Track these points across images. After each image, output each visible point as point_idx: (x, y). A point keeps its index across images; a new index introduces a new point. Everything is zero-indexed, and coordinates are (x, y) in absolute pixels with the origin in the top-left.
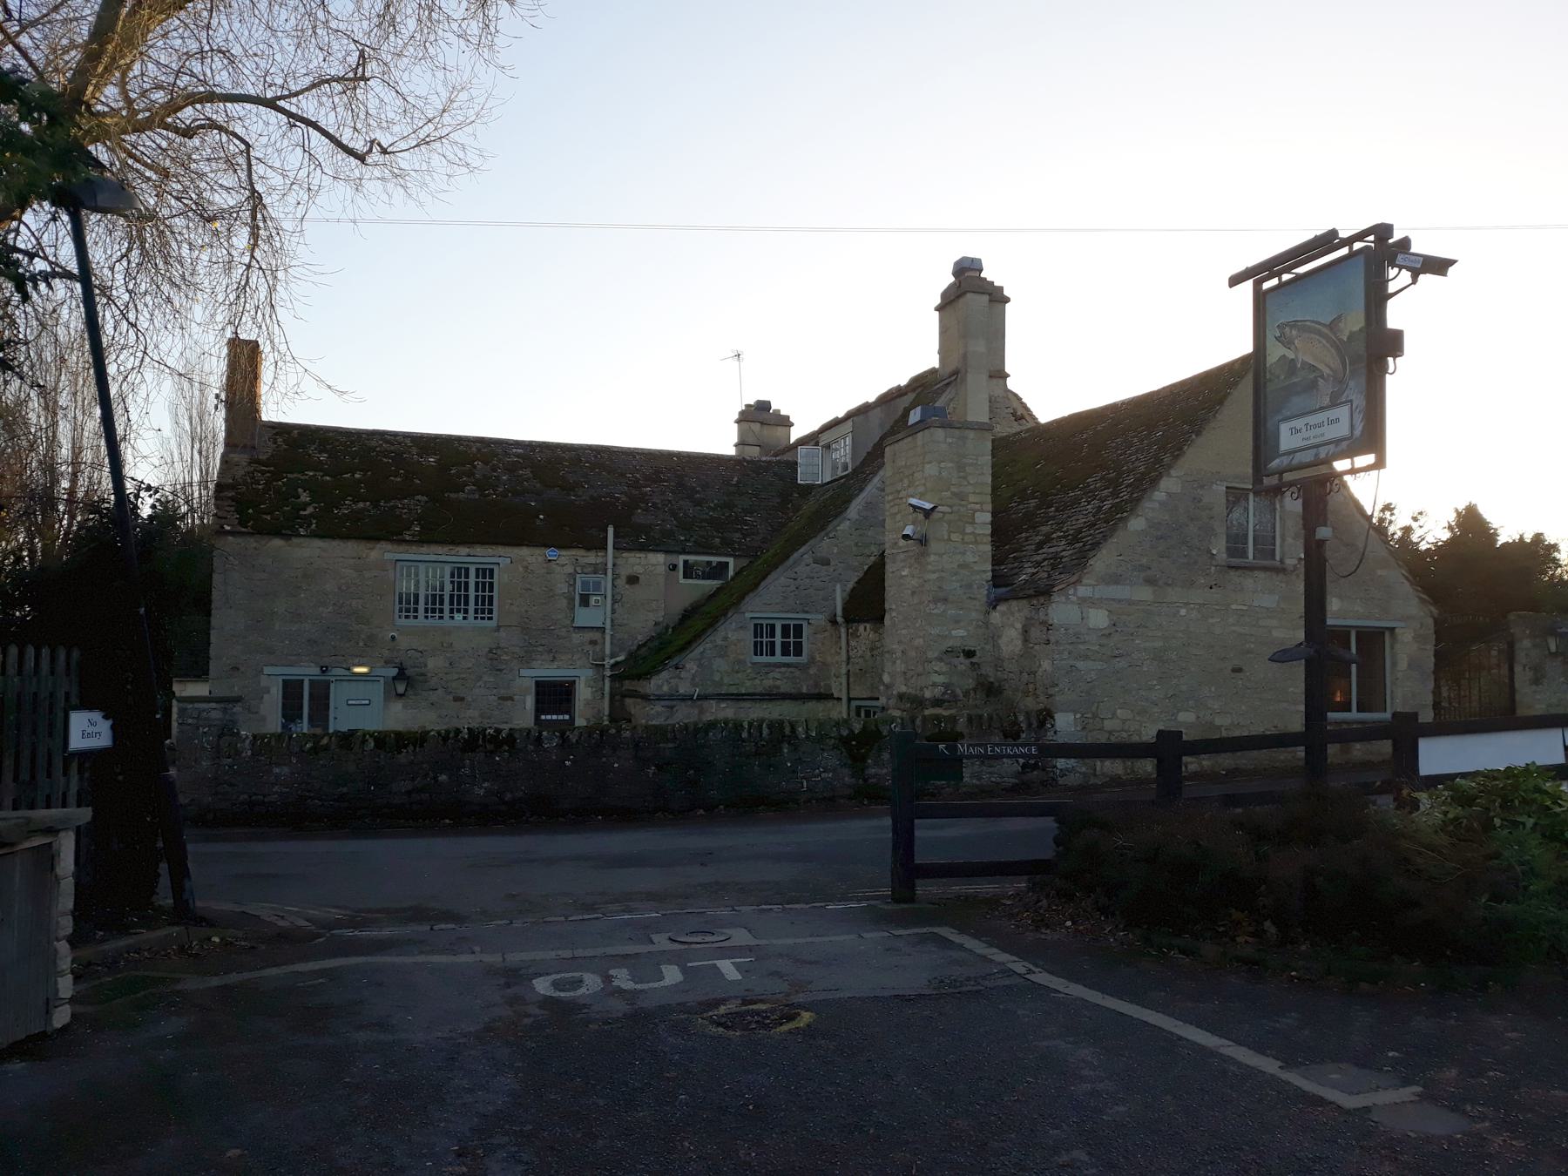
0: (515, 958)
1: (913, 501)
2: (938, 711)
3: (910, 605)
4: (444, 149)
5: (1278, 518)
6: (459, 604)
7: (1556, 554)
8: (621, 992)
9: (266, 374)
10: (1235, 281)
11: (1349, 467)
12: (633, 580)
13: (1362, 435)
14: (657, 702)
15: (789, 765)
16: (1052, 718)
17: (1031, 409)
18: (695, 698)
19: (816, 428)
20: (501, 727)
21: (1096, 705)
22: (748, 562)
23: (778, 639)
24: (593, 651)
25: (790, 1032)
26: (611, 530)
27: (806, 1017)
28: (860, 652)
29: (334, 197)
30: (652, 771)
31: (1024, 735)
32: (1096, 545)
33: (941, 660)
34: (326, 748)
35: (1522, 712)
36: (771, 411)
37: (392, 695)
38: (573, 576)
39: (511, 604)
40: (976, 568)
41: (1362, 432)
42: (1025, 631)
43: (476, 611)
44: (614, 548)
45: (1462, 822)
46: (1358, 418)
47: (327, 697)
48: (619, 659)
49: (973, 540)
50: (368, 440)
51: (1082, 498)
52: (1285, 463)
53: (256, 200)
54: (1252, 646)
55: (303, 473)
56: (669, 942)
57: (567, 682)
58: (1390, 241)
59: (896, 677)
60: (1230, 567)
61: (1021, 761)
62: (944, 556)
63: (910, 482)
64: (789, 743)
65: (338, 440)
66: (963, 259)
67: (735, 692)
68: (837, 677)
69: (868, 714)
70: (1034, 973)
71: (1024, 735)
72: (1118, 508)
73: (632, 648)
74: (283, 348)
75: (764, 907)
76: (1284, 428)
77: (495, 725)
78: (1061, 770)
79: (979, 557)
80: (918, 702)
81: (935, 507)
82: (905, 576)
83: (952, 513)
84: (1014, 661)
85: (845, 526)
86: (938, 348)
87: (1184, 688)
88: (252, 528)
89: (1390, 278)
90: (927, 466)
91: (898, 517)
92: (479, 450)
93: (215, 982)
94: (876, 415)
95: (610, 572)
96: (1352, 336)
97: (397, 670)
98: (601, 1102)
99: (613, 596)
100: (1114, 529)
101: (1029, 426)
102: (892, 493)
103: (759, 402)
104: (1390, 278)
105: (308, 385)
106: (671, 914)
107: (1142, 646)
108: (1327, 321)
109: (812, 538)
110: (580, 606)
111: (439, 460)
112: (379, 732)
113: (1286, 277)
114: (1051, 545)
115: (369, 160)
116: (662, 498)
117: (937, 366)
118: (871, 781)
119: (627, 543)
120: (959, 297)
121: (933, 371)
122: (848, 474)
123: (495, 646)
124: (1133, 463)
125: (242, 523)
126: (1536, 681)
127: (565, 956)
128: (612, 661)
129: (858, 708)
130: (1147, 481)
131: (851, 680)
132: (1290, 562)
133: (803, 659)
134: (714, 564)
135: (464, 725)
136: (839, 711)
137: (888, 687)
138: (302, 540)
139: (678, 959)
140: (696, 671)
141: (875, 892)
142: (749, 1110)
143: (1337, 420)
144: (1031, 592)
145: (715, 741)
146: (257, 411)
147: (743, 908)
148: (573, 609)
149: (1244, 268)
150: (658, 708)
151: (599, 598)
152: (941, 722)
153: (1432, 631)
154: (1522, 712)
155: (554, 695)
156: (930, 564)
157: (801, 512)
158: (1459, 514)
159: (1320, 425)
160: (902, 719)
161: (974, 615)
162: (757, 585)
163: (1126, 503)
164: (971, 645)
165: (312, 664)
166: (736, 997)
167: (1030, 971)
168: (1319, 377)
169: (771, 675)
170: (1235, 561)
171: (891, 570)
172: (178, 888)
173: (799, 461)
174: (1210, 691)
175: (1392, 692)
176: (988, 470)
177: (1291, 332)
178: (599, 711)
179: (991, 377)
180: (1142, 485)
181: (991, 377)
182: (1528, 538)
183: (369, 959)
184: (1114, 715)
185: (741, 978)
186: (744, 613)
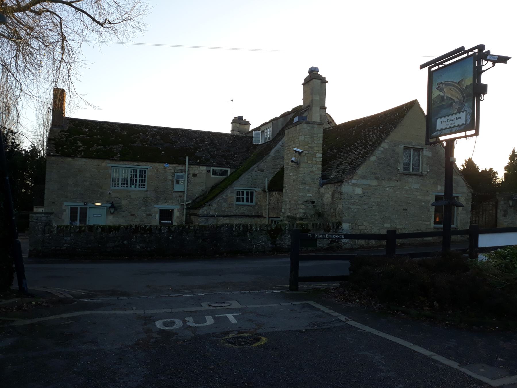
0: (149, 312)
1: (295, 149)
2: (301, 222)
3: (292, 185)
4: (132, 23)
5: (421, 158)
6: (133, 182)
7: (497, 175)
8: (190, 327)
9: (67, 99)
10: (422, 67)
11: (464, 135)
12: (195, 175)
13: (470, 123)
14: (202, 217)
15: (249, 240)
16: (341, 225)
17: (334, 120)
18: (215, 216)
19: (259, 126)
20: (147, 225)
21: (356, 221)
22: (235, 170)
23: (245, 197)
24: (180, 200)
25: (258, 346)
26: (187, 158)
27: (264, 340)
28: (273, 201)
29: (93, 36)
30: (201, 241)
31: (331, 231)
32: (359, 166)
33: (302, 204)
34: (84, 231)
35: (500, 226)
36: (243, 120)
37: (109, 213)
38: (173, 173)
39: (152, 183)
40: (316, 173)
41: (470, 122)
42: (333, 195)
43: (139, 185)
44: (188, 164)
45: (502, 265)
46: (469, 117)
47: (86, 213)
48: (189, 202)
49: (316, 163)
50: (102, 124)
51: (353, 150)
52: (438, 134)
53: (64, 38)
54: (410, 201)
55: (79, 135)
56: (208, 306)
57: (171, 210)
58: (484, 51)
59: (286, 210)
60: (404, 174)
61: (330, 240)
62: (305, 169)
63: (294, 143)
64: (250, 232)
65: (92, 125)
66: (312, 68)
67: (229, 214)
68: (265, 210)
69: (275, 222)
70: (349, 321)
71: (331, 231)
72: (366, 153)
73: (194, 199)
74: (73, 91)
75: (243, 292)
76: (439, 121)
77: (145, 224)
78: (344, 243)
79: (317, 169)
80: (294, 218)
81: (303, 151)
82: (291, 175)
83: (308, 153)
84: (328, 205)
85: (269, 158)
86: (302, 98)
87: (387, 215)
88: (61, 154)
89: (483, 65)
90: (300, 137)
91: (289, 155)
92: (142, 129)
93: (28, 322)
94: (280, 121)
95: (187, 172)
96: (467, 87)
97: (111, 204)
98: (183, 381)
99: (188, 181)
100: (365, 160)
101: (333, 125)
102: (287, 146)
103: (239, 117)
104: (483, 65)
105: (82, 103)
106: (208, 294)
107: (373, 201)
108: (457, 81)
109: (258, 162)
110: (176, 184)
111: (128, 132)
112: (103, 226)
113: (441, 66)
114: (342, 165)
115: (104, 26)
116: (205, 147)
117: (302, 104)
118: (278, 246)
119: (193, 163)
120: (310, 80)
121: (300, 106)
122: (270, 141)
123: (146, 197)
124: (372, 137)
125: (57, 152)
126: (505, 215)
127: (168, 311)
128: (187, 203)
129: (272, 221)
130: (377, 144)
131: (270, 211)
132: (424, 173)
133: (253, 203)
134: (223, 171)
135: (134, 224)
136: (266, 221)
137: (283, 213)
138: (78, 158)
139: (212, 313)
140: (216, 207)
141: (283, 286)
142: (245, 385)
143: (460, 118)
144: (336, 181)
145: (223, 231)
146: (64, 114)
147: (235, 292)
148: (173, 185)
149: (426, 62)
150: (203, 219)
151: (183, 181)
152: (303, 226)
153: (471, 198)
154: (500, 226)
155: (166, 214)
156: (300, 171)
157: (254, 153)
158: (466, 161)
159: (453, 120)
160: (289, 224)
161: (315, 189)
162: (238, 178)
163: (369, 151)
164: (314, 199)
165: (81, 202)
166: (235, 330)
167: (347, 320)
168: (454, 102)
169: (242, 209)
170: (406, 172)
171: (286, 173)
172: (20, 283)
173: (253, 136)
174: (396, 216)
175: (456, 217)
176: (321, 139)
177: (442, 86)
178: (182, 220)
179: (321, 108)
180: (375, 145)
181: (321, 108)
182: (488, 170)
183: (93, 312)
184: (362, 225)
185: (236, 322)
186: (233, 187)
